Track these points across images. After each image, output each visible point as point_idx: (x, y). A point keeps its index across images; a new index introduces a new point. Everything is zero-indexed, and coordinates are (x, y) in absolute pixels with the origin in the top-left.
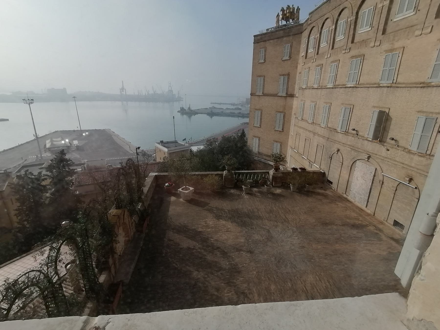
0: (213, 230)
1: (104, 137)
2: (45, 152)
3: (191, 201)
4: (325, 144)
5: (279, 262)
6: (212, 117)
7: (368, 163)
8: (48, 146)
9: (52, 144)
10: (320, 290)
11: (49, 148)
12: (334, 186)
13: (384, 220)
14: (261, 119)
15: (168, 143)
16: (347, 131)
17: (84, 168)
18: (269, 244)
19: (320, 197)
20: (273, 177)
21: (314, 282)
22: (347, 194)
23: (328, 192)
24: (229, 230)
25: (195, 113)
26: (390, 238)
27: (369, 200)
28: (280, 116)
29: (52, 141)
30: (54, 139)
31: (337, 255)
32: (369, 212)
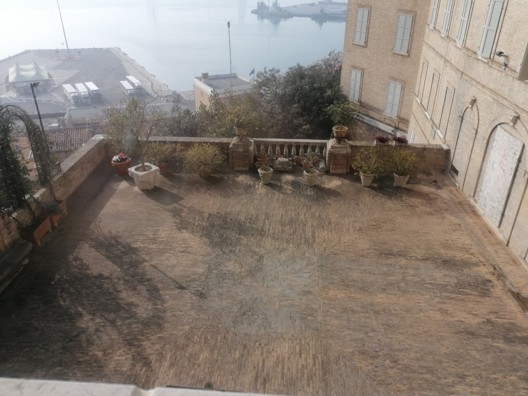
0: (161, 247)
1: (105, 63)
2: (8, 91)
3: (153, 192)
4: (457, 87)
5: (244, 314)
6: (321, 24)
7: (514, 132)
8: (12, 78)
9: (18, 75)
10: (289, 369)
11: (13, 83)
12: (460, 179)
13: (520, 256)
14: (368, 28)
15: (217, 77)
16: (492, 57)
17: (63, 121)
18: (247, 281)
19: (415, 201)
20: (331, 154)
21: (287, 355)
22: (476, 198)
23: (443, 193)
24: (189, 249)
25: (288, 14)
26: (513, 293)
27: (506, 213)
28: (405, 20)
29: (18, 70)
30: (22, 67)
31: (367, 312)
32: (501, 236)
